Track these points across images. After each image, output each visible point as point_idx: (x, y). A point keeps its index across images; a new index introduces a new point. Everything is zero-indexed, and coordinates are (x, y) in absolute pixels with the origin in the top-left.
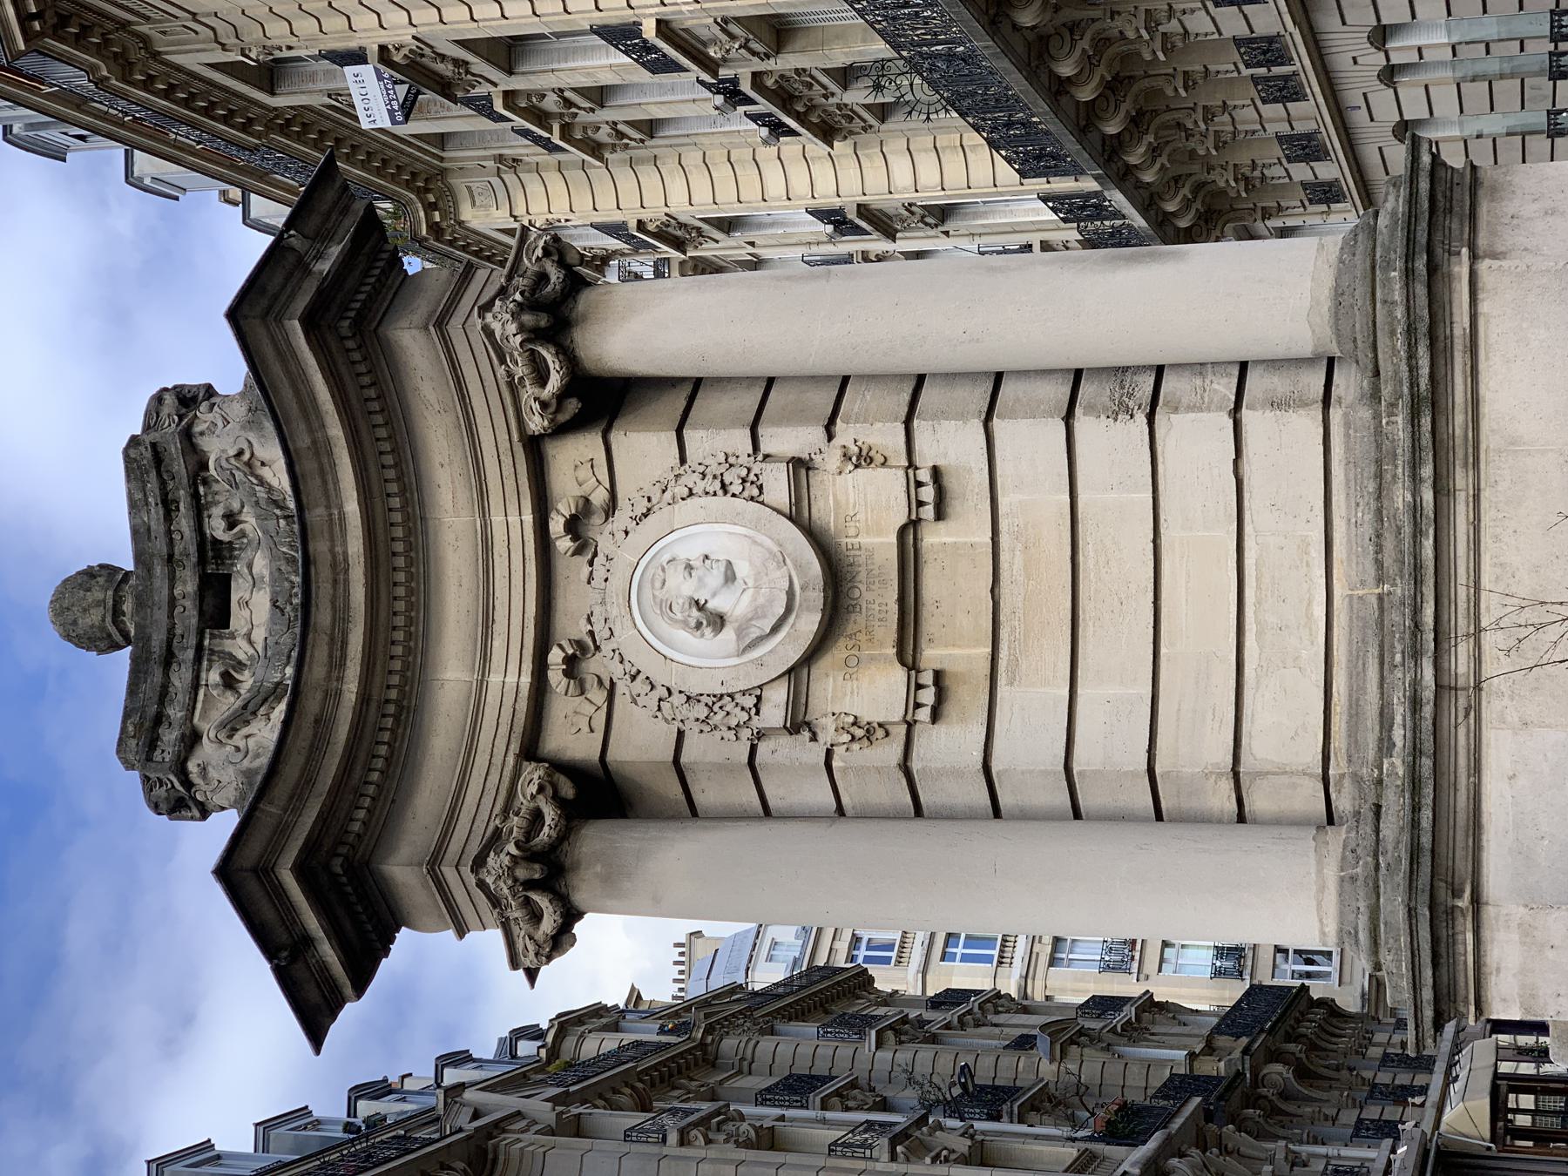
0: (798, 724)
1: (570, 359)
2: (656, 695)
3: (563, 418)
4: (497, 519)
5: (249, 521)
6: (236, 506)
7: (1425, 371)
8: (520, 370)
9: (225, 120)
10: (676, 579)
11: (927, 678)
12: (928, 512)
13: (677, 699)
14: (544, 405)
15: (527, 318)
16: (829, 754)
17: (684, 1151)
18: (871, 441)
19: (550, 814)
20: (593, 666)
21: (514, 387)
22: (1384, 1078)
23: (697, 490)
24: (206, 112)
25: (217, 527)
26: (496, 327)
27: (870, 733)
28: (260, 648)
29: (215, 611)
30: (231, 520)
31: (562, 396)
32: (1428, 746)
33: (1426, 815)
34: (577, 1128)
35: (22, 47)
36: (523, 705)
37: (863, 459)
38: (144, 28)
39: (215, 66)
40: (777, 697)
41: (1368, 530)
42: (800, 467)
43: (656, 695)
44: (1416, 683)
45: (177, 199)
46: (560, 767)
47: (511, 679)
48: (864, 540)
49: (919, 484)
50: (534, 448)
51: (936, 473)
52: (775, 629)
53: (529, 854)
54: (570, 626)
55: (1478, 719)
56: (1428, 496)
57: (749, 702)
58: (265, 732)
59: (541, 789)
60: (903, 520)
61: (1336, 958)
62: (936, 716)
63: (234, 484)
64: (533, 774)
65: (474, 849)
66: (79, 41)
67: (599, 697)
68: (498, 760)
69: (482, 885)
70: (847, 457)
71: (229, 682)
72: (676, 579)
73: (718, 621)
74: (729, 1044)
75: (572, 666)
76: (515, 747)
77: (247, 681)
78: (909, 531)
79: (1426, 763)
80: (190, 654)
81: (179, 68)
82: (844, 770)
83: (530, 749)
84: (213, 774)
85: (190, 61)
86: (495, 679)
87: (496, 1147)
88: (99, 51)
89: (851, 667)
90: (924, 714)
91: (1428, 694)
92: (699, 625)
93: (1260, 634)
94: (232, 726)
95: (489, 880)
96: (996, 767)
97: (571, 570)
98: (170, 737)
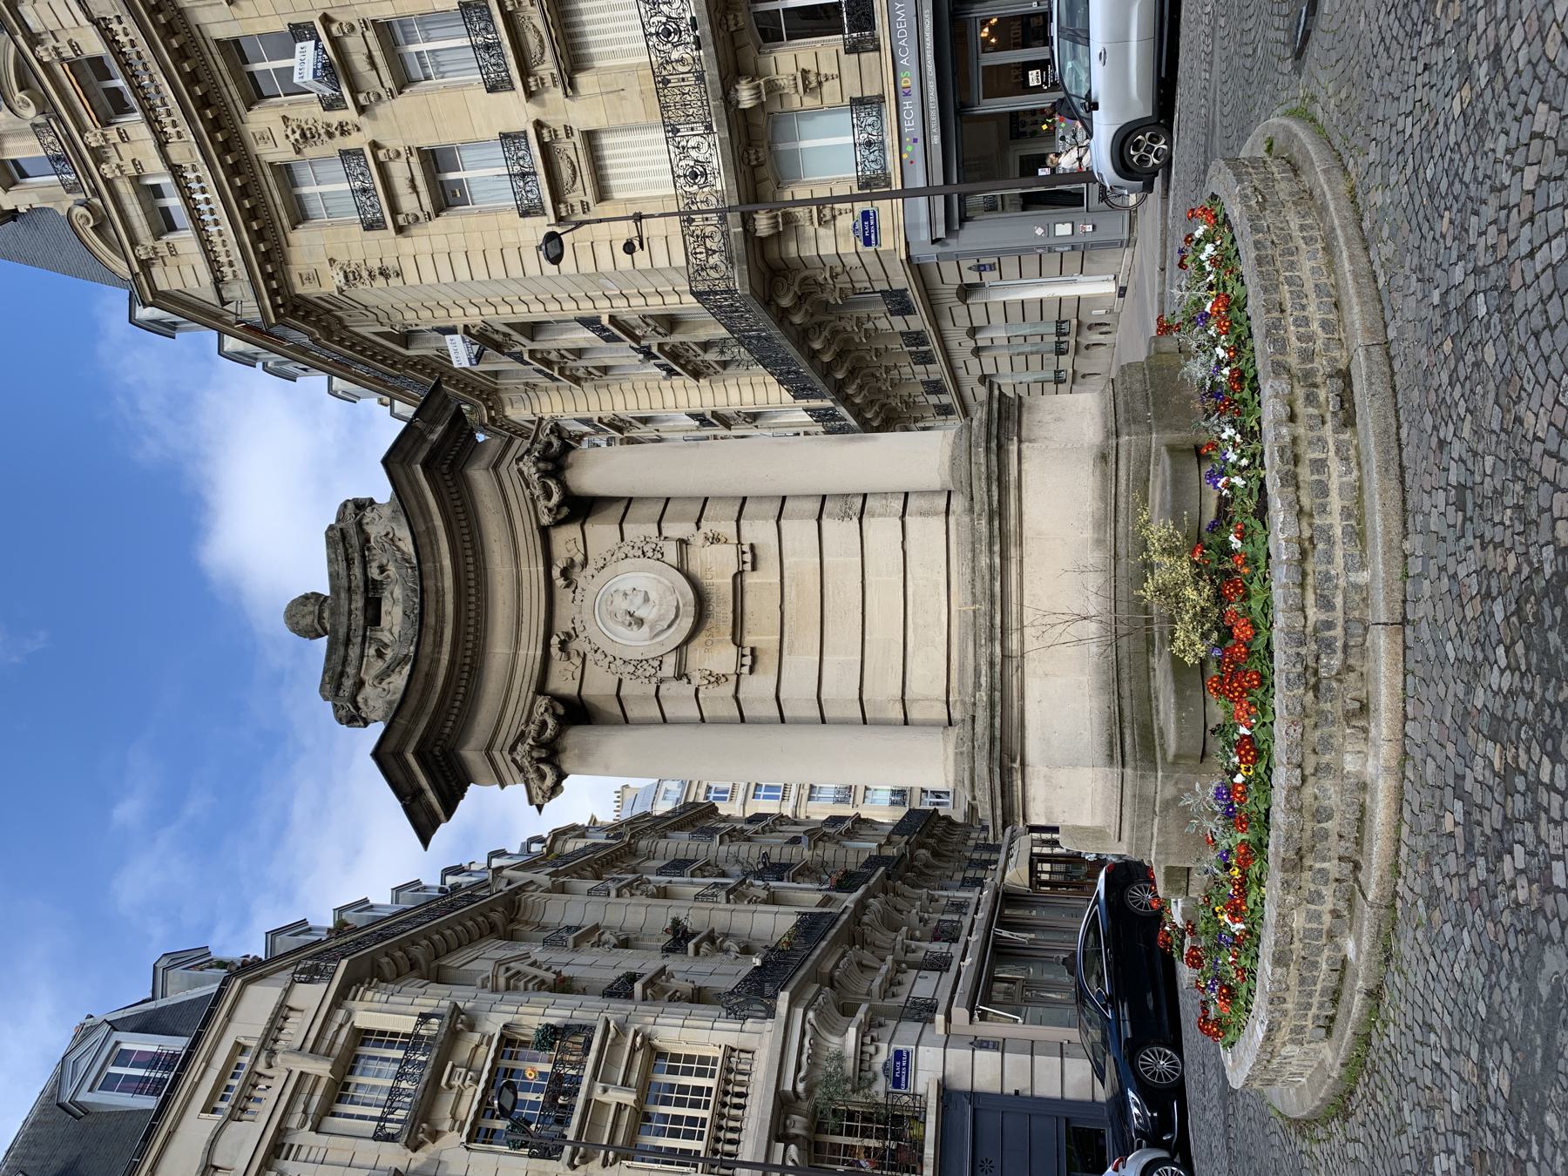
0: (681, 675)
1: (563, 486)
2: (607, 660)
3: (560, 517)
4: (524, 568)
5: (392, 570)
6: (385, 562)
7: (996, 498)
8: (538, 492)
10: (618, 600)
11: (747, 651)
12: (748, 567)
13: (619, 662)
14: (550, 510)
15: (541, 465)
16: (697, 690)
17: (619, 900)
19: (551, 723)
20: (574, 645)
22: (976, 856)
24: (372, 357)
25: (374, 573)
26: (525, 469)
27: (718, 679)
30: (382, 569)
31: (559, 506)
32: (998, 686)
33: (998, 721)
34: (562, 889)
36: (537, 666)
37: (715, 539)
38: (339, 313)
40: (670, 661)
41: (968, 577)
43: (607, 660)
44: (992, 654)
46: (557, 698)
47: (531, 652)
49: (743, 553)
50: (545, 533)
51: (752, 547)
52: (670, 626)
54: (562, 625)
55: (1023, 672)
56: (997, 560)
57: (656, 664)
58: (399, 681)
59: (546, 710)
61: (951, 795)
62: (751, 671)
64: (542, 702)
65: (510, 741)
66: (304, 319)
67: (578, 661)
68: (523, 695)
71: (380, 655)
72: (618, 600)
73: (640, 622)
74: (643, 844)
75: (563, 646)
76: (533, 688)
77: (389, 653)
78: (739, 574)
79: (997, 694)
80: (360, 639)
81: (357, 334)
83: (541, 689)
84: (371, 703)
85: (364, 331)
86: (522, 652)
88: (315, 325)
90: (746, 670)
91: (998, 660)
92: (630, 624)
94: (381, 678)
95: (518, 758)
97: (563, 595)
98: (348, 683)
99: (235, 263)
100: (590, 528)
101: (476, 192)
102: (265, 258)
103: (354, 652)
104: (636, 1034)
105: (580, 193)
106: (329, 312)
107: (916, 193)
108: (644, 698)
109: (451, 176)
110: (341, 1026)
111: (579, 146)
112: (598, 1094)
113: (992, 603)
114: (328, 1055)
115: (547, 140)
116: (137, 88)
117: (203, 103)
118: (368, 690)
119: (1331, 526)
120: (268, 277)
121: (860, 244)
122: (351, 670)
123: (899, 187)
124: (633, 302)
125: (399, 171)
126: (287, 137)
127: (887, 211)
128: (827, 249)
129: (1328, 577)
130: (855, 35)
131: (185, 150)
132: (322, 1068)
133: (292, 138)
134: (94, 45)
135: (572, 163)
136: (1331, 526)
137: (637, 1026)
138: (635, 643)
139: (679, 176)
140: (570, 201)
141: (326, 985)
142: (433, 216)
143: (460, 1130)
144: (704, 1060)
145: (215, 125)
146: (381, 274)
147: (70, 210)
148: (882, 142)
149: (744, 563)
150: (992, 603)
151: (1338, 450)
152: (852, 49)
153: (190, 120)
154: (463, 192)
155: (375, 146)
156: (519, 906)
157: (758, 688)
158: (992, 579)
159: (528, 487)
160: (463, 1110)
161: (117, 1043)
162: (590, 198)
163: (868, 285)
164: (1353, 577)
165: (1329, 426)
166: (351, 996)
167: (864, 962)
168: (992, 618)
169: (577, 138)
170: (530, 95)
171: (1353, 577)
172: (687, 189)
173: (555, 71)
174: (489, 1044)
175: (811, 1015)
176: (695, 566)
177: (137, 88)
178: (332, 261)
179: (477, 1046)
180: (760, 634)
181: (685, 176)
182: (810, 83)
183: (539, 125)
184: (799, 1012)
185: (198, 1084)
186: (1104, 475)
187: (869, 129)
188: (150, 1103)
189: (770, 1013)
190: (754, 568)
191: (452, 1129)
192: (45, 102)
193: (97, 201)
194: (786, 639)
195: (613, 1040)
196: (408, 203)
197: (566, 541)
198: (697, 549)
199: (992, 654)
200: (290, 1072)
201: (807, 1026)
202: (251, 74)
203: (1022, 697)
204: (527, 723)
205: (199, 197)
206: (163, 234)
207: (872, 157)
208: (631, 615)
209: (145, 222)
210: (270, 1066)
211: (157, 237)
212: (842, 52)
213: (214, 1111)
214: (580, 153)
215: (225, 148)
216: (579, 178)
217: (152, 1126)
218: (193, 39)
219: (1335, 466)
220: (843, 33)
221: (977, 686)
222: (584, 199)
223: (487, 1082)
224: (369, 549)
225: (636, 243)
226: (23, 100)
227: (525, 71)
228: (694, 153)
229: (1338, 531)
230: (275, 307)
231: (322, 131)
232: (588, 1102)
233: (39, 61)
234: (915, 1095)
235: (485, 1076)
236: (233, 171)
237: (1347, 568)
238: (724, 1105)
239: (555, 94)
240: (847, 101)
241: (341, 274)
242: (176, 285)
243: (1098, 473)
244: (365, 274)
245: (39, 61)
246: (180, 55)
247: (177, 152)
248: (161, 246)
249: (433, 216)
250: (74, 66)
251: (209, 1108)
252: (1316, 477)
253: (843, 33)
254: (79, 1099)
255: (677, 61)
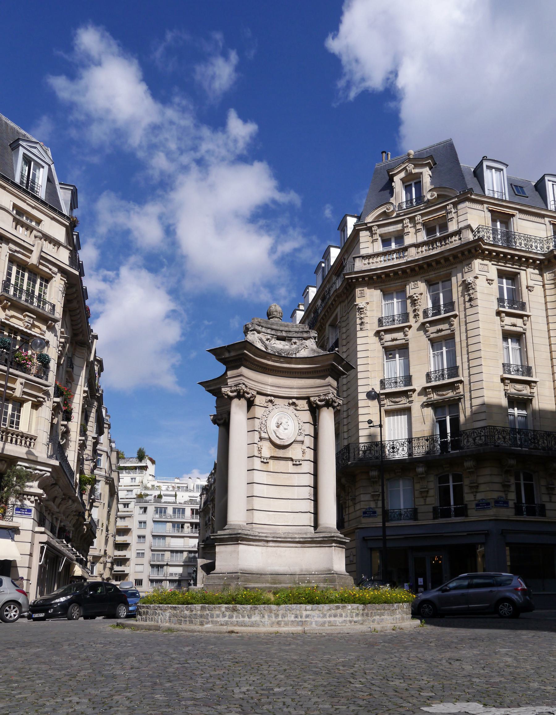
0: (261, 438)
2: (266, 415)
4: (295, 390)
5: (294, 346)
6: (297, 344)
8: (322, 398)
9: (325, 315)
10: (286, 420)
11: (268, 461)
12: (294, 463)
13: (266, 419)
14: (315, 401)
15: (331, 400)
16: (256, 444)
17: (82, 392)
18: (306, 454)
19: (249, 396)
20: (270, 404)
21: (319, 396)
23: (300, 425)
24: (327, 311)
25: (294, 340)
26: (330, 395)
27: (260, 450)
28: (273, 345)
29: (279, 338)
30: (295, 343)
31: (317, 404)
32: (260, 538)
35: (346, 277)
36: (265, 392)
37: (304, 453)
38: (346, 301)
39: (337, 315)
40: (266, 436)
42: (302, 442)
43: (266, 415)
45: (303, 296)
47: (269, 390)
48: (290, 452)
49: (299, 461)
50: (308, 398)
51: (301, 464)
52: (277, 436)
53: (244, 392)
54: (276, 401)
56: (297, 540)
57: (265, 431)
58: (259, 345)
59: (253, 395)
60: (293, 458)
62: (262, 462)
63: (302, 344)
64: (255, 393)
65: (246, 383)
66: (346, 288)
67: (265, 405)
69: (240, 384)
70: (304, 450)
71: (268, 339)
72: (286, 420)
73: (278, 427)
75: (271, 401)
76: (259, 390)
77: (267, 342)
78: (292, 460)
80: (273, 333)
81: (337, 307)
82: (254, 446)
83: (259, 393)
84: (253, 335)
85: (338, 309)
86: (269, 387)
87: (85, 347)
88: (343, 291)
89: (270, 448)
90: (262, 460)
92: (278, 423)
93: (274, 514)
94: (261, 340)
95: (240, 385)
96: (254, 471)
97: (286, 401)
98: (259, 328)
99: (369, 266)
100: (309, 412)
101: (391, 363)
102: (371, 277)
103: (269, 331)
104: (44, 399)
105: (388, 404)
106: (347, 297)
107: (384, 532)
108: (254, 426)
109: (397, 356)
110: (50, 270)
111: (406, 405)
112: (20, 380)
113: (284, 538)
114: (40, 263)
115: (409, 393)
116: (436, 241)
117: (429, 265)
118: (257, 335)
119: (326, 618)
120: (363, 277)
121: (364, 510)
122: (264, 330)
123: (386, 525)
124: (345, 420)
125: (400, 335)
126: (415, 294)
127: (378, 521)
128: (363, 498)
129: (313, 616)
130: (439, 511)
131: (413, 254)
132: (33, 259)
133: (414, 296)
134: (453, 227)
135: (400, 402)
136: (326, 618)
137: (46, 399)
138: (272, 425)
139: (393, 442)
140: (385, 401)
141: (68, 264)
142: (383, 346)
143: (6, 319)
144: (18, 424)
145: (421, 267)
146: (362, 322)
147: (392, 204)
148: (401, 520)
149: (296, 461)
150: (284, 538)
151: (345, 620)
152: (435, 509)
153: (424, 258)
154: (391, 358)
155: (410, 327)
156: (82, 346)
157: (257, 463)
158: (291, 538)
159: (323, 395)
160: (13, 320)
161: (43, 167)
162: (386, 407)
163: (347, 513)
164: (314, 623)
165: (351, 619)
166: (63, 275)
167: (57, 499)
168: (280, 538)
169: (408, 405)
170: (425, 389)
171: (314, 623)
172: (388, 445)
173: (433, 399)
174: (41, 334)
175: (49, 474)
176: (294, 445)
177: (436, 241)
178: (368, 303)
179: (40, 329)
180: (273, 465)
181: (393, 445)
182: (424, 494)
183: (414, 391)
184: (50, 470)
185: (25, 202)
186: (323, 571)
187: (406, 515)
188: (42, 194)
189: (50, 457)
190: (294, 465)
191: (6, 315)
192: (432, 203)
193: (395, 215)
194: (271, 473)
195: (42, 388)
196: (388, 337)
197: (303, 404)
198: (301, 447)
199: (269, 537)
200: (33, 246)
201: (44, 472)
202: (438, 283)
203: (256, 546)
204: (250, 389)
205: (395, 256)
206: (381, 238)
207: (396, 515)
208: (281, 424)
209: (386, 232)
210: (36, 237)
211: (381, 235)
212: (433, 506)
213: (13, 208)
214: (403, 406)
215: (412, 269)
216: (394, 404)
217: (9, 180)
218: (452, 264)
219: (341, 619)
220: (440, 506)
221: (259, 533)
222: (386, 405)
223: (26, 332)
224: (302, 340)
225: (371, 425)
226: (434, 195)
227: (435, 389)
228: (401, 449)
229: (325, 619)
230: (352, 278)
231: (416, 307)
232: (17, 376)
233: (448, 205)
234: (12, 516)
235: (29, 331)
236: (404, 271)
237: (316, 621)
238: (12, 434)
239: (424, 399)
240: (416, 507)
241: (363, 307)
242: (362, 240)
243: (324, 569)
244: (362, 316)
245: (448, 205)
246: (446, 259)
247: (412, 251)
248: (377, 236)
249: (383, 346)
250: (444, 217)
251: (15, 206)
252: (338, 615)
253: (440, 506)
254: (20, 147)
255: (434, 445)
